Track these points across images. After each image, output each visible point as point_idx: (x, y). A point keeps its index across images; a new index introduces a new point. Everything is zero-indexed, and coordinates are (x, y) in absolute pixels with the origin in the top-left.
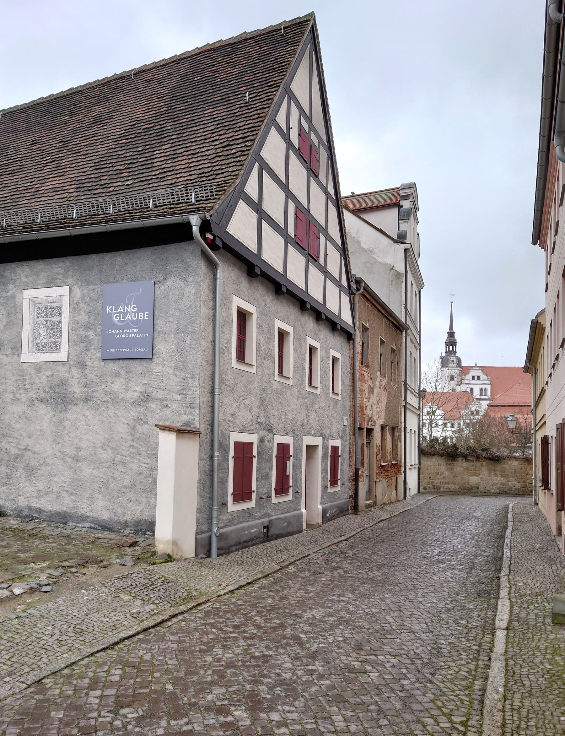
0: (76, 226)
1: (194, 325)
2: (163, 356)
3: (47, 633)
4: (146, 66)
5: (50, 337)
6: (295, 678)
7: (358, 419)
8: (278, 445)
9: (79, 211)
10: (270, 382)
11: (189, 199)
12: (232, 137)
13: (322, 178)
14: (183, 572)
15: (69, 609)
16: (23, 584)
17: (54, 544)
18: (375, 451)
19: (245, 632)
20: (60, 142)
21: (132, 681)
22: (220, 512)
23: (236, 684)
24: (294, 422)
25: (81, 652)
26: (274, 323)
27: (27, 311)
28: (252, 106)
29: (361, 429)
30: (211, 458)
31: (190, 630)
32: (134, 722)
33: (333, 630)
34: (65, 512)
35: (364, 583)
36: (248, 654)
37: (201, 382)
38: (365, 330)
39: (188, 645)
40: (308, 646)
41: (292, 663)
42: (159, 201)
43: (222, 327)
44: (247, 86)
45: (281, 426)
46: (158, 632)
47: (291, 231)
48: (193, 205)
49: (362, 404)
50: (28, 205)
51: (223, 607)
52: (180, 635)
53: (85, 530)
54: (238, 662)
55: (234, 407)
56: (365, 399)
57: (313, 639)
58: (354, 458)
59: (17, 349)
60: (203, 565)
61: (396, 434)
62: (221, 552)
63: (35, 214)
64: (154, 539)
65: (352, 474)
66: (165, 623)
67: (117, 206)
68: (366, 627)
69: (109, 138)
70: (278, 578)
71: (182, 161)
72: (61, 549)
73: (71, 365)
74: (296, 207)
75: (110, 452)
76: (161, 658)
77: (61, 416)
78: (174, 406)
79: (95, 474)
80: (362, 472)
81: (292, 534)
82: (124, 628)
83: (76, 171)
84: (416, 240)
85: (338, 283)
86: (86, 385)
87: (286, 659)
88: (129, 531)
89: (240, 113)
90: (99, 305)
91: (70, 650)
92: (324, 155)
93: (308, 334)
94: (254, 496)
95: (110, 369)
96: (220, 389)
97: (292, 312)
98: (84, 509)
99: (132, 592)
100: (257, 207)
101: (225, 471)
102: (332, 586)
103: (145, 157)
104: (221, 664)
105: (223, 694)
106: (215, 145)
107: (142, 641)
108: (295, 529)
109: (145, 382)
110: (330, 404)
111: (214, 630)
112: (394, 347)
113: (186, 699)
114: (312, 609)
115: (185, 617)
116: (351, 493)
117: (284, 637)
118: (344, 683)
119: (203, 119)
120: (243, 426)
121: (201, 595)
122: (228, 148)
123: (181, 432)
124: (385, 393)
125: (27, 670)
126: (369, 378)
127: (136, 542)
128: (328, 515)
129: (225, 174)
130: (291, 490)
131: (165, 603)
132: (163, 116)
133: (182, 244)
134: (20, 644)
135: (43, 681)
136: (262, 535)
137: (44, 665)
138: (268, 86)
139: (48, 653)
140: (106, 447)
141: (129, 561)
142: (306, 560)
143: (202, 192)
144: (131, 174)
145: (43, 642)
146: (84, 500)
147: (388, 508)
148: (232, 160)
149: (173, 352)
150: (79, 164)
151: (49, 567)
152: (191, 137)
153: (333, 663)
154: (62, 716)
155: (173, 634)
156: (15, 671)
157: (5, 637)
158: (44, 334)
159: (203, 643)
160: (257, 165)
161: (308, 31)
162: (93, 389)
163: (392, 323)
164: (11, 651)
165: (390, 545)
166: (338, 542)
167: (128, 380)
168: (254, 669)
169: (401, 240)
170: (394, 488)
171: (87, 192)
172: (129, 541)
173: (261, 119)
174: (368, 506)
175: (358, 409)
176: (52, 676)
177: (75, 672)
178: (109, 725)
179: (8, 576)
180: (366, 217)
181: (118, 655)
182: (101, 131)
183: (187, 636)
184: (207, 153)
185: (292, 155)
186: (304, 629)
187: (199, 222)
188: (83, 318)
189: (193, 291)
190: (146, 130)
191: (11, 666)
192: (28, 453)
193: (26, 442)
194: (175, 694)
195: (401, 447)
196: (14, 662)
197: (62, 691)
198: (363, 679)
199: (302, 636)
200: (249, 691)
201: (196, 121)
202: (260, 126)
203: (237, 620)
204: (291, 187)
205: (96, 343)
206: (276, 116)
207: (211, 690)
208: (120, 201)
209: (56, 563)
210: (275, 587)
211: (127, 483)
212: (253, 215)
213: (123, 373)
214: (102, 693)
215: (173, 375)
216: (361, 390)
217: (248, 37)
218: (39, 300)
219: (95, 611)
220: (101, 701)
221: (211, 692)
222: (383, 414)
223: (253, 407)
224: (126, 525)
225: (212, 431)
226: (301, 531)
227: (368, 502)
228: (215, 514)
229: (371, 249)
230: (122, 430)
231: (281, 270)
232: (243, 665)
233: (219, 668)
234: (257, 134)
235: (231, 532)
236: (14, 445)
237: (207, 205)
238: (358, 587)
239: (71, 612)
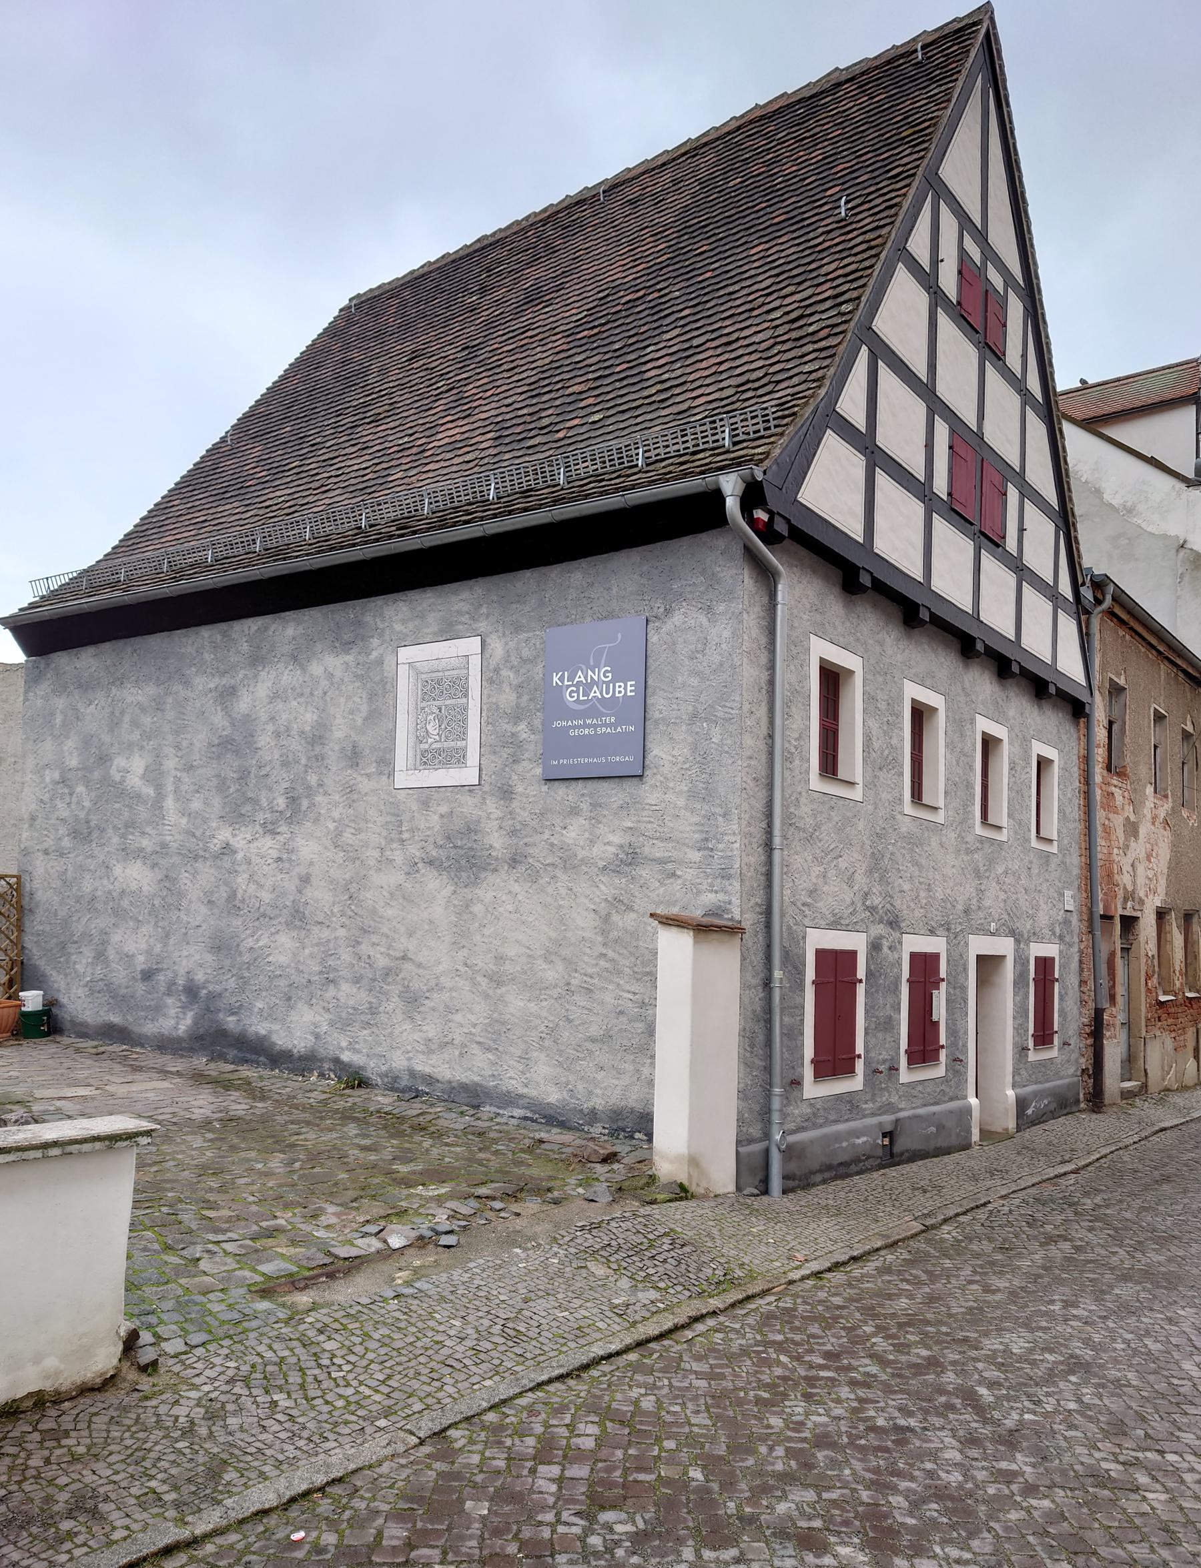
0: (495, 516)
1: (728, 704)
2: (665, 770)
3: (452, 1333)
6: (969, 1485)
7: (1101, 896)
8: (913, 956)
9: (500, 485)
11: (717, 441)
12: (810, 297)
13: (1013, 359)
14: (711, 1223)
15: (494, 1287)
16: (405, 1227)
17: (458, 1149)
18: (1143, 968)
19: (850, 1368)
20: (463, 349)
21: (619, 1453)
22: (786, 1098)
23: (838, 1485)
24: (949, 906)
25: (517, 1380)
26: (901, 690)
27: (473, 757)
28: (854, 226)
29: (1107, 918)
30: (767, 984)
31: (735, 1354)
32: (629, 1544)
33: (1055, 1384)
34: (477, 1084)
35: (1125, 1278)
36: (860, 1419)
37: (744, 823)
38: (1116, 691)
39: (730, 1385)
40: (996, 1415)
41: (961, 1452)
42: (657, 451)
43: (787, 704)
44: (843, 184)
45: (919, 913)
46: (667, 1351)
47: (941, 486)
48: (728, 452)
49: (1111, 862)
50: (406, 481)
51: (801, 1308)
52: (712, 1362)
53: (514, 1122)
54: (840, 1436)
55: (814, 875)
56: (1116, 851)
57: (1009, 1401)
58: (1091, 984)
59: (386, 764)
60: (754, 1212)
62: (791, 1184)
63: (418, 499)
64: (651, 1148)
65: (1086, 1021)
66: (679, 1333)
67: (573, 468)
68: (1134, 1383)
69: (557, 330)
70: (918, 1251)
71: (702, 360)
72: (471, 1160)
73: (486, 793)
74: (952, 432)
75: (560, 967)
76: (677, 1408)
77: (468, 893)
78: (689, 874)
79: (533, 1010)
80: (1112, 1015)
81: (947, 1151)
82: (598, 1335)
83: (493, 405)
85: (1050, 592)
86: (513, 833)
87: (947, 1440)
88: (600, 1130)
90: (539, 669)
91: (497, 1373)
92: (1015, 309)
93: (980, 708)
94: (860, 1065)
95: (559, 798)
96: (784, 837)
97: (944, 662)
98: (512, 1082)
99: (612, 1259)
100: (865, 442)
101: (797, 1011)
102: (1047, 1280)
103: (629, 362)
104: (803, 1435)
105: (812, 1505)
106: (772, 320)
107: (636, 1368)
108: (954, 1141)
109: (630, 824)
110: (1031, 862)
111: (783, 1358)
112: (1189, 728)
113: (731, 1505)
114: (1002, 1329)
115: (720, 1323)
116: (1085, 1063)
117: (941, 1391)
118: (1085, 1510)
120: (834, 915)
121: (751, 1276)
122: (801, 323)
123: (706, 929)
124: (1168, 833)
125: (418, 1406)
126: (1127, 801)
127: (615, 1154)
128: (1029, 1112)
129: (795, 380)
130: (943, 1054)
131: (679, 1288)
132: (665, 271)
133: (704, 537)
134: (404, 1352)
135: (449, 1433)
136: (880, 1152)
137: (448, 1400)
138: (889, 178)
139: (456, 1375)
140: (553, 957)
141: (601, 1191)
142: (982, 1215)
143: (745, 423)
144: (599, 400)
145: (445, 1351)
146: (512, 1062)
147: (1178, 1099)
148: (810, 347)
149: (684, 763)
150: (499, 390)
151: (451, 1196)
152: (722, 308)
153: (1057, 1461)
154: (486, 1512)
155: (698, 1358)
156: (397, 1408)
157: (376, 1336)
159: (762, 1385)
160: (864, 351)
161: (977, 46)
162: (526, 840)
163: (1184, 671)
164: (388, 1364)
165: (1185, 1191)
166: (1056, 1176)
167: (595, 820)
168: (876, 1456)
170: (1191, 1053)
171: (515, 446)
172: (602, 1152)
173: (873, 252)
174: (1127, 1095)
175: (1099, 873)
176: (464, 1425)
177: (508, 1420)
178: (578, 1543)
179: (378, 1209)
180: (1118, 432)
181: (589, 1392)
182: (539, 317)
183: (727, 1366)
184: (756, 339)
186: (986, 1374)
187: (740, 488)
188: (507, 698)
189: (727, 634)
190: (630, 305)
191: (388, 1396)
192: (408, 966)
193: (404, 943)
194: (709, 1491)
196: (395, 1389)
197: (484, 1459)
198: (1131, 1505)
199: (983, 1391)
200: (868, 1504)
201: (733, 273)
202: (872, 266)
203: (833, 1340)
204: (942, 390)
205: (532, 747)
206: (907, 240)
207: (784, 1491)
208: (580, 456)
209: (464, 1188)
210: (914, 1272)
211: (594, 1030)
212: (855, 459)
213: (584, 806)
214: (562, 1471)
215: (686, 809)
216: (1107, 831)
217: (843, 78)
218: (425, 667)
219: (541, 1293)
220: (560, 1488)
221: (784, 1497)
222: (1163, 882)
223: (856, 875)
224: (593, 1116)
225: (768, 926)
226: (966, 1147)
227: (1127, 1085)
228: (776, 1103)
229: (1129, 504)
230: (584, 922)
232: (851, 1444)
233: (799, 1445)
234: (864, 286)
235: (812, 1141)
236: (383, 950)
237: (756, 451)
238: (1112, 1287)
239: (495, 1293)
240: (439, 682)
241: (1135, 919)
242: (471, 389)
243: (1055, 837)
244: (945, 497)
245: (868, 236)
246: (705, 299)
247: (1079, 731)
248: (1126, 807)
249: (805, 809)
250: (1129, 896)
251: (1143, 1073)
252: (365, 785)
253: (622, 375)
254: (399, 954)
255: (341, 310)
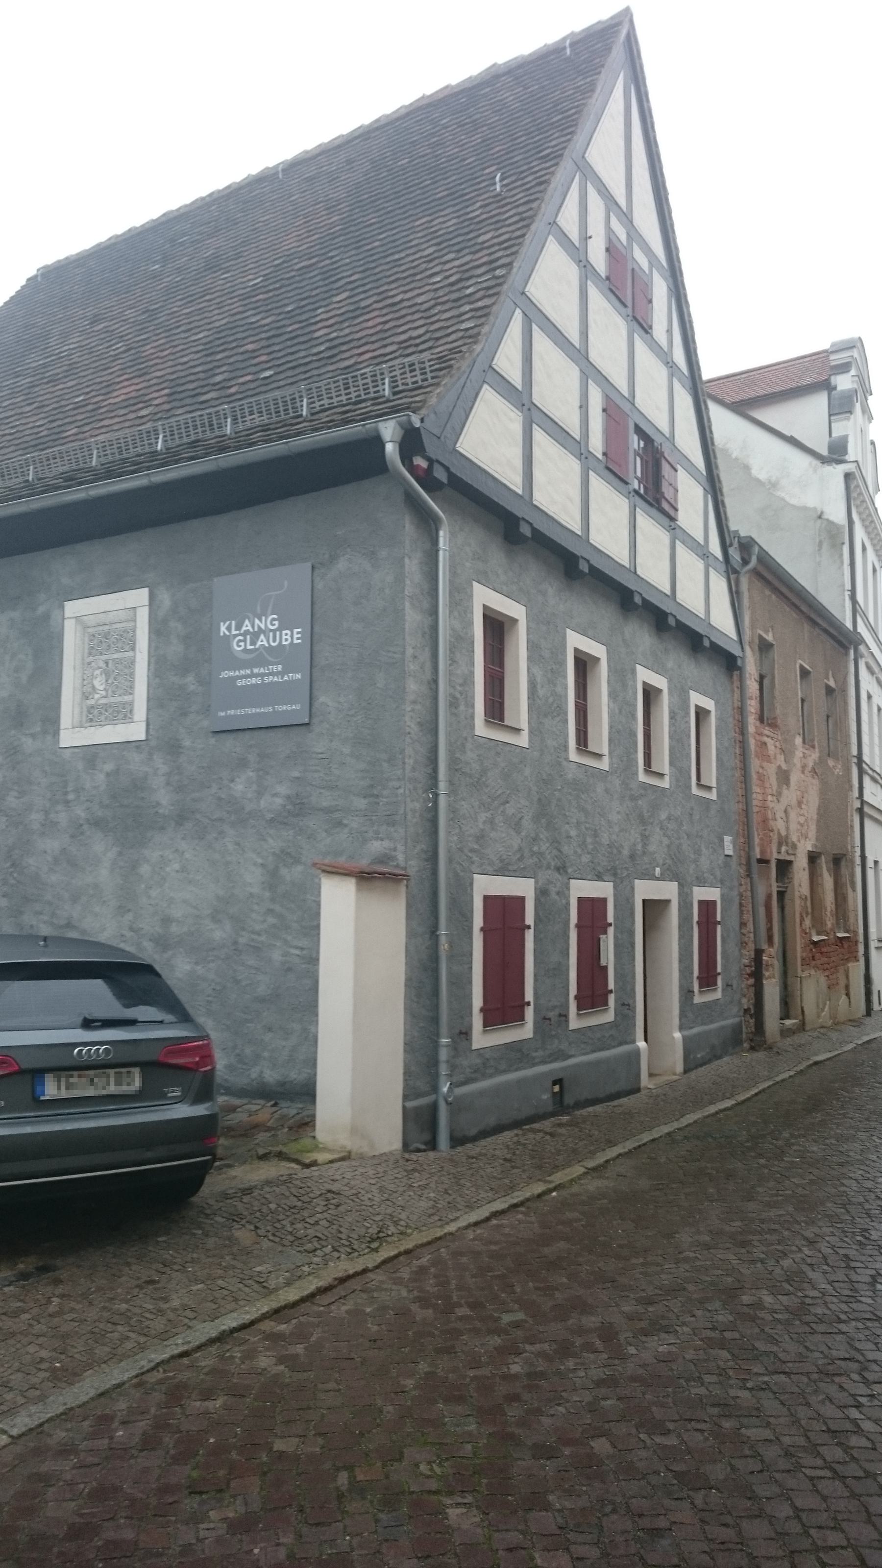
4: (306, 152)
5: (114, 692)
7: (757, 840)
10: (559, 764)
11: (378, 391)
13: (659, 331)
18: (798, 909)
20: (144, 313)
24: (615, 851)
28: (508, 200)
29: (763, 861)
38: (764, 647)
45: (586, 859)
47: (596, 444)
48: (388, 401)
49: (766, 808)
56: (770, 798)
59: (52, 723)
61: (844, 871)
71: (368, 320)
78: (355, 823)
80: (770, 956)
84: (870, 456)
85: (703, 553)
89: (484, 216)
92: (660, 289)
97: (605, 614)
100: (521, 398)
103: (300, 322)
112: (832, 683)
116: (747, 1003)
119: (411, 237)
120: (502, 861)
122: (460, 285)
123: (366, 878)
124: (816, 782)
126: (778, 751)
130: (612, 999)
149: (350, 709)
158: (102, 688)
160: (518, 314)
169: (834, 456)
170: (843, 992)
171: (188, 401)
173: (525, 223)
175: (756, 819)
185: (593, 292)
187: (400, 433)
189: (390, 578)
195: (855, 901)
204: (594, 356)
206: (557, 215)
212: (512, 415)
213: (252, 758)
216: (761, 778)
218: (91, 621)
222: (813, 828)
227: (788, 1022)
228: (443, 1055)
230: (252, 878)
231: (576, 527)
236: (46, 918)
240: (107, 635)
241: (790, 863)
242: (149, 349)
243: (714, 784)
244: (600, 456)
245: (521, 209)
246: (373, 265)
247: (732, 683)
248: (778, 756)
249: (470, 755)
250: (783, 841)
251: (800, 1012)
252: (28, 744)
253: (294, 334)
254: (63, 922)
255: (28, 280)
